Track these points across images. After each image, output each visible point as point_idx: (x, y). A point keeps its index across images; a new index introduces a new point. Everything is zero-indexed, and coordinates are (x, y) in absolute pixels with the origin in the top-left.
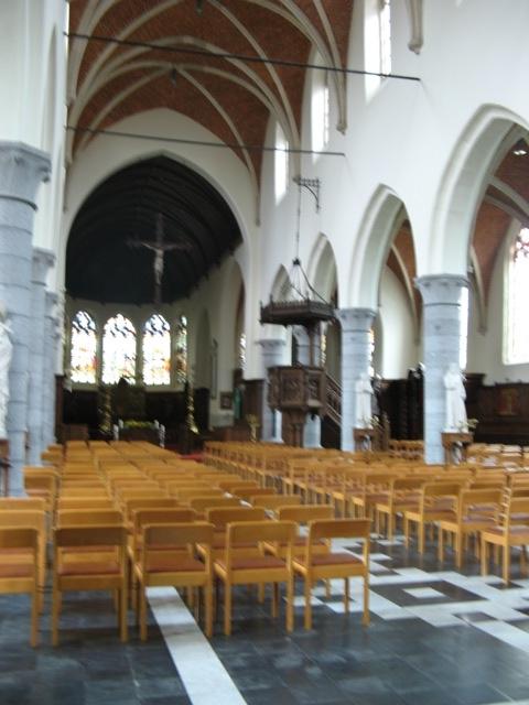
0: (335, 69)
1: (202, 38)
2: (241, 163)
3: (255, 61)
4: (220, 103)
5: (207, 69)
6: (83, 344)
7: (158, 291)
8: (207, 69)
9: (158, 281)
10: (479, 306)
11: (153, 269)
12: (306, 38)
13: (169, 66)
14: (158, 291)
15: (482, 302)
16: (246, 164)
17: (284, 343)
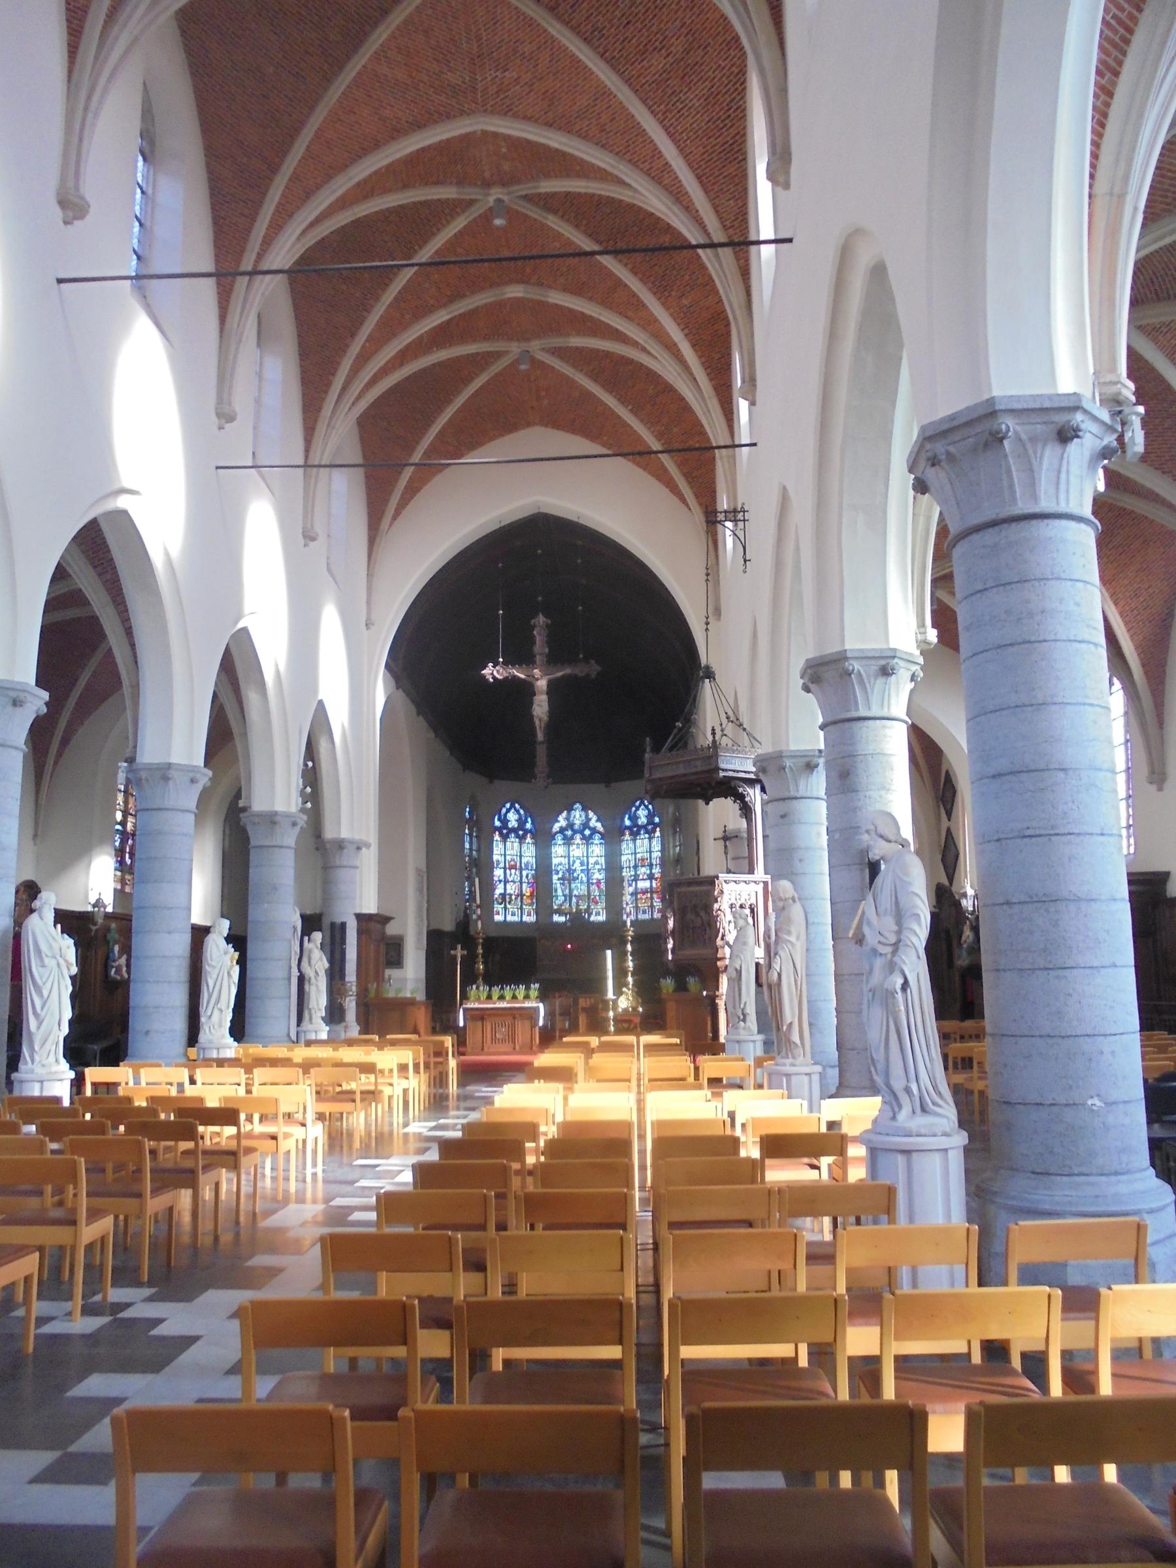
0: (713, 246)
1: (540, 284)
2: (675, 500)
3: (632, 307)
4: (623, 401)
5: (577, 341)
6: (511, 855)
7: (541, 753)
8: (577, 341)
9: (540, 736)
10: (1143, 726)
11: (531, 717)
12: (183, 32)
13: (515, 348)
14: (541, 753)
15: (1150, 716)
16: (684, 500)
17: (368, 846)
